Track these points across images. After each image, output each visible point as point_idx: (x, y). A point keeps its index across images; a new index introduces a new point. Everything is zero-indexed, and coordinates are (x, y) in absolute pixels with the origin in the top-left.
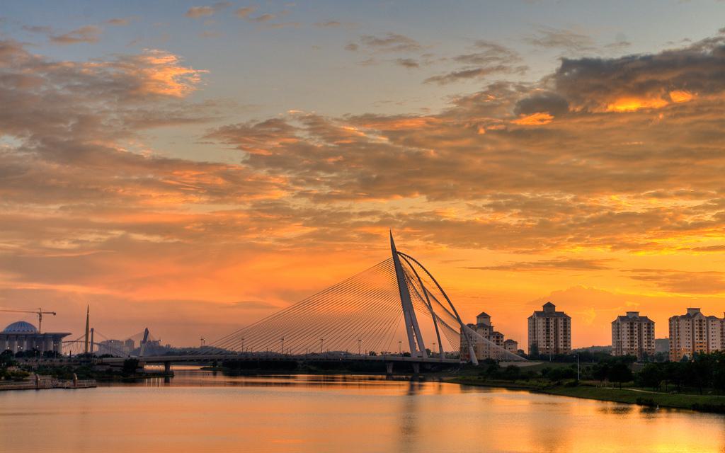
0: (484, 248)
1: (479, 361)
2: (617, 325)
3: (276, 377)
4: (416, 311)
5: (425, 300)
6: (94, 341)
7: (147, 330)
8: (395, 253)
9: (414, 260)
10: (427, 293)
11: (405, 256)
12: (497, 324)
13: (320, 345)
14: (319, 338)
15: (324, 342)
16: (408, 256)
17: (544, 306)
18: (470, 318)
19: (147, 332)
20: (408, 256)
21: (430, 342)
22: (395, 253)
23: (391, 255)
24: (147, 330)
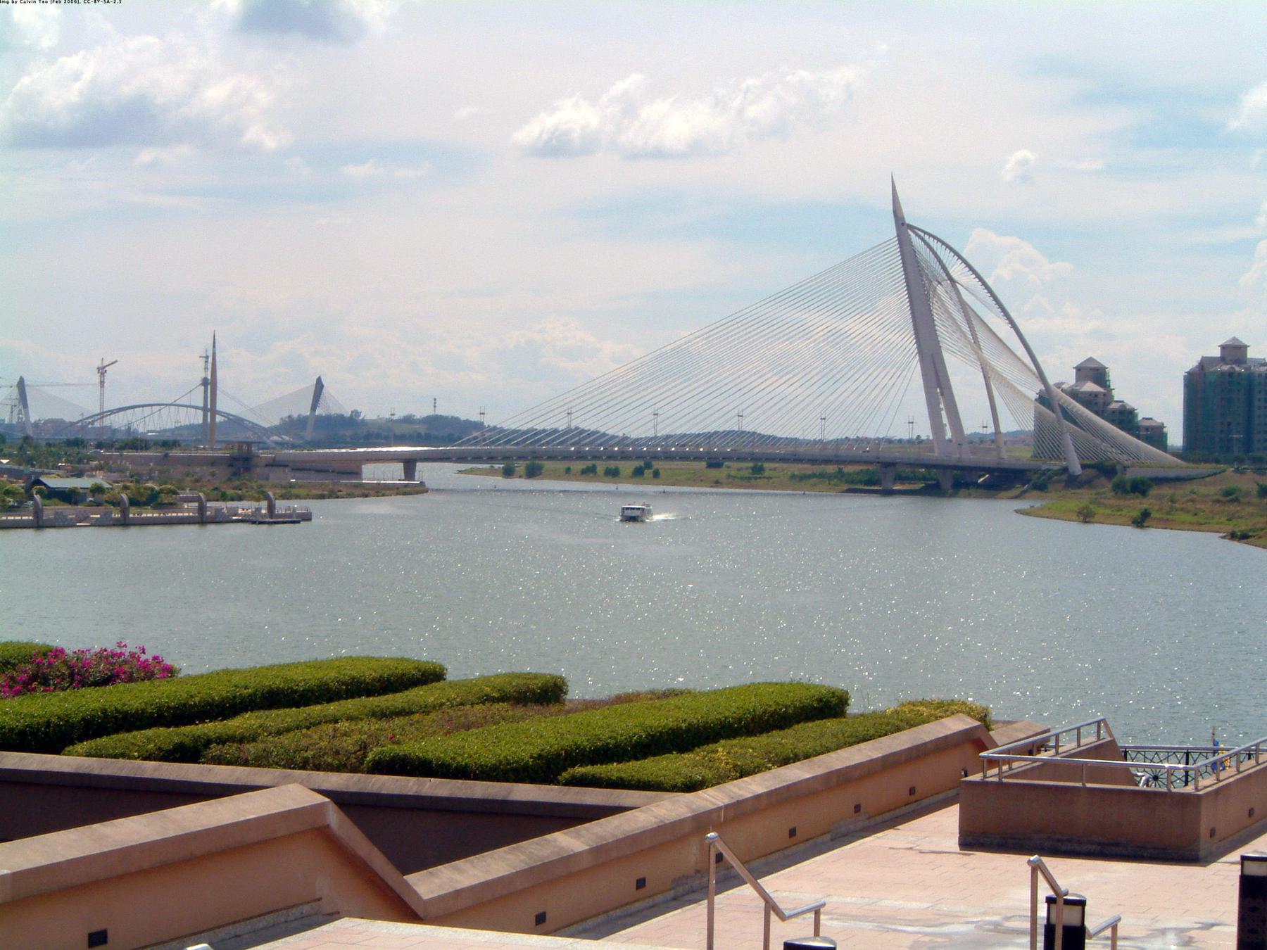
0: (418, 417)
1: (1084, 467)
2: (352, 412)
3: (1016, 746)
4: (947, 356)
5: (966, 328)
6: (219, 408)
7: (319, 380)
8: (902, 225)
9: (943, 243)
10: (971, 314)
11: (922, 233)
12: (1123, 392)
13: (651, 424)
14: (651, 410)
15: (659, 419)
16: (930, 235)
17: (1223, 347)
18: (1062, 373)
19: (319, 386)
20: (935, 238)
21: (975, 420)
22: (902, 225)
23: (892, 232)
24: (319, 380)
